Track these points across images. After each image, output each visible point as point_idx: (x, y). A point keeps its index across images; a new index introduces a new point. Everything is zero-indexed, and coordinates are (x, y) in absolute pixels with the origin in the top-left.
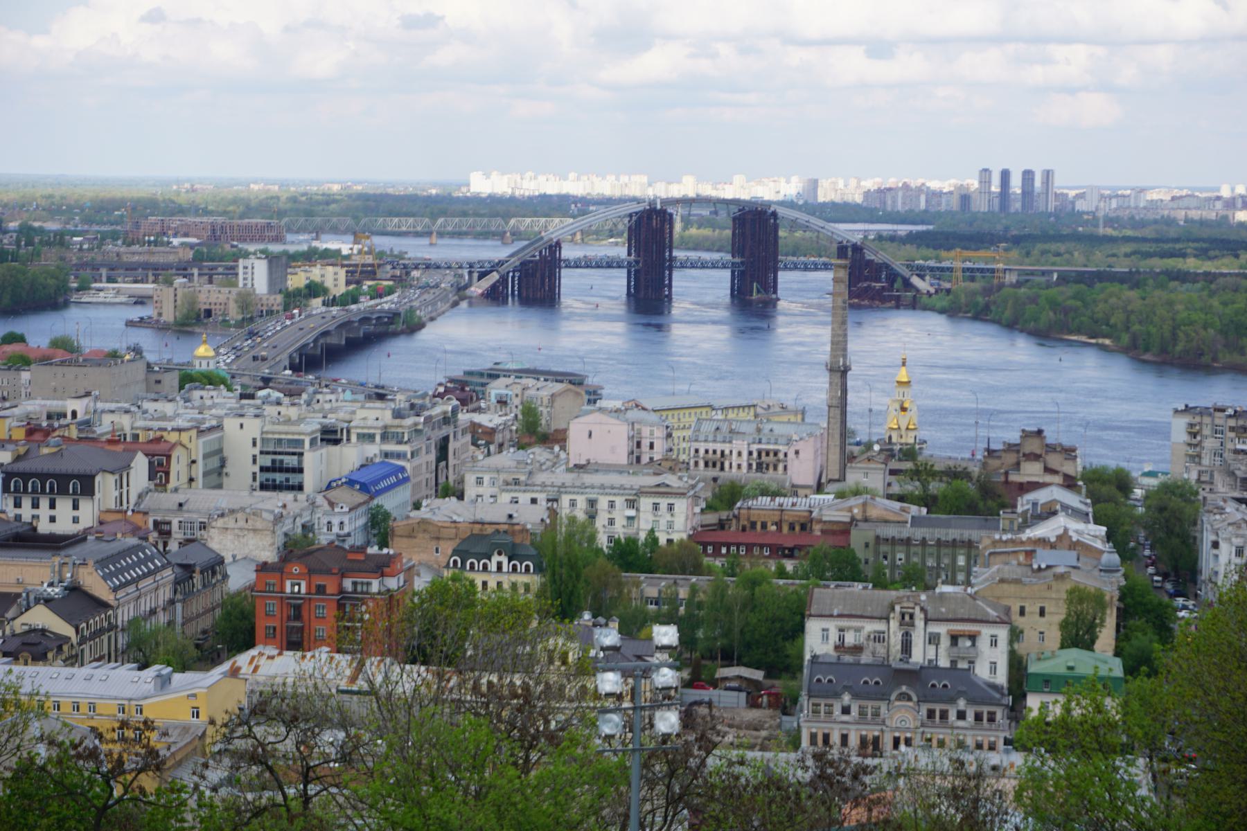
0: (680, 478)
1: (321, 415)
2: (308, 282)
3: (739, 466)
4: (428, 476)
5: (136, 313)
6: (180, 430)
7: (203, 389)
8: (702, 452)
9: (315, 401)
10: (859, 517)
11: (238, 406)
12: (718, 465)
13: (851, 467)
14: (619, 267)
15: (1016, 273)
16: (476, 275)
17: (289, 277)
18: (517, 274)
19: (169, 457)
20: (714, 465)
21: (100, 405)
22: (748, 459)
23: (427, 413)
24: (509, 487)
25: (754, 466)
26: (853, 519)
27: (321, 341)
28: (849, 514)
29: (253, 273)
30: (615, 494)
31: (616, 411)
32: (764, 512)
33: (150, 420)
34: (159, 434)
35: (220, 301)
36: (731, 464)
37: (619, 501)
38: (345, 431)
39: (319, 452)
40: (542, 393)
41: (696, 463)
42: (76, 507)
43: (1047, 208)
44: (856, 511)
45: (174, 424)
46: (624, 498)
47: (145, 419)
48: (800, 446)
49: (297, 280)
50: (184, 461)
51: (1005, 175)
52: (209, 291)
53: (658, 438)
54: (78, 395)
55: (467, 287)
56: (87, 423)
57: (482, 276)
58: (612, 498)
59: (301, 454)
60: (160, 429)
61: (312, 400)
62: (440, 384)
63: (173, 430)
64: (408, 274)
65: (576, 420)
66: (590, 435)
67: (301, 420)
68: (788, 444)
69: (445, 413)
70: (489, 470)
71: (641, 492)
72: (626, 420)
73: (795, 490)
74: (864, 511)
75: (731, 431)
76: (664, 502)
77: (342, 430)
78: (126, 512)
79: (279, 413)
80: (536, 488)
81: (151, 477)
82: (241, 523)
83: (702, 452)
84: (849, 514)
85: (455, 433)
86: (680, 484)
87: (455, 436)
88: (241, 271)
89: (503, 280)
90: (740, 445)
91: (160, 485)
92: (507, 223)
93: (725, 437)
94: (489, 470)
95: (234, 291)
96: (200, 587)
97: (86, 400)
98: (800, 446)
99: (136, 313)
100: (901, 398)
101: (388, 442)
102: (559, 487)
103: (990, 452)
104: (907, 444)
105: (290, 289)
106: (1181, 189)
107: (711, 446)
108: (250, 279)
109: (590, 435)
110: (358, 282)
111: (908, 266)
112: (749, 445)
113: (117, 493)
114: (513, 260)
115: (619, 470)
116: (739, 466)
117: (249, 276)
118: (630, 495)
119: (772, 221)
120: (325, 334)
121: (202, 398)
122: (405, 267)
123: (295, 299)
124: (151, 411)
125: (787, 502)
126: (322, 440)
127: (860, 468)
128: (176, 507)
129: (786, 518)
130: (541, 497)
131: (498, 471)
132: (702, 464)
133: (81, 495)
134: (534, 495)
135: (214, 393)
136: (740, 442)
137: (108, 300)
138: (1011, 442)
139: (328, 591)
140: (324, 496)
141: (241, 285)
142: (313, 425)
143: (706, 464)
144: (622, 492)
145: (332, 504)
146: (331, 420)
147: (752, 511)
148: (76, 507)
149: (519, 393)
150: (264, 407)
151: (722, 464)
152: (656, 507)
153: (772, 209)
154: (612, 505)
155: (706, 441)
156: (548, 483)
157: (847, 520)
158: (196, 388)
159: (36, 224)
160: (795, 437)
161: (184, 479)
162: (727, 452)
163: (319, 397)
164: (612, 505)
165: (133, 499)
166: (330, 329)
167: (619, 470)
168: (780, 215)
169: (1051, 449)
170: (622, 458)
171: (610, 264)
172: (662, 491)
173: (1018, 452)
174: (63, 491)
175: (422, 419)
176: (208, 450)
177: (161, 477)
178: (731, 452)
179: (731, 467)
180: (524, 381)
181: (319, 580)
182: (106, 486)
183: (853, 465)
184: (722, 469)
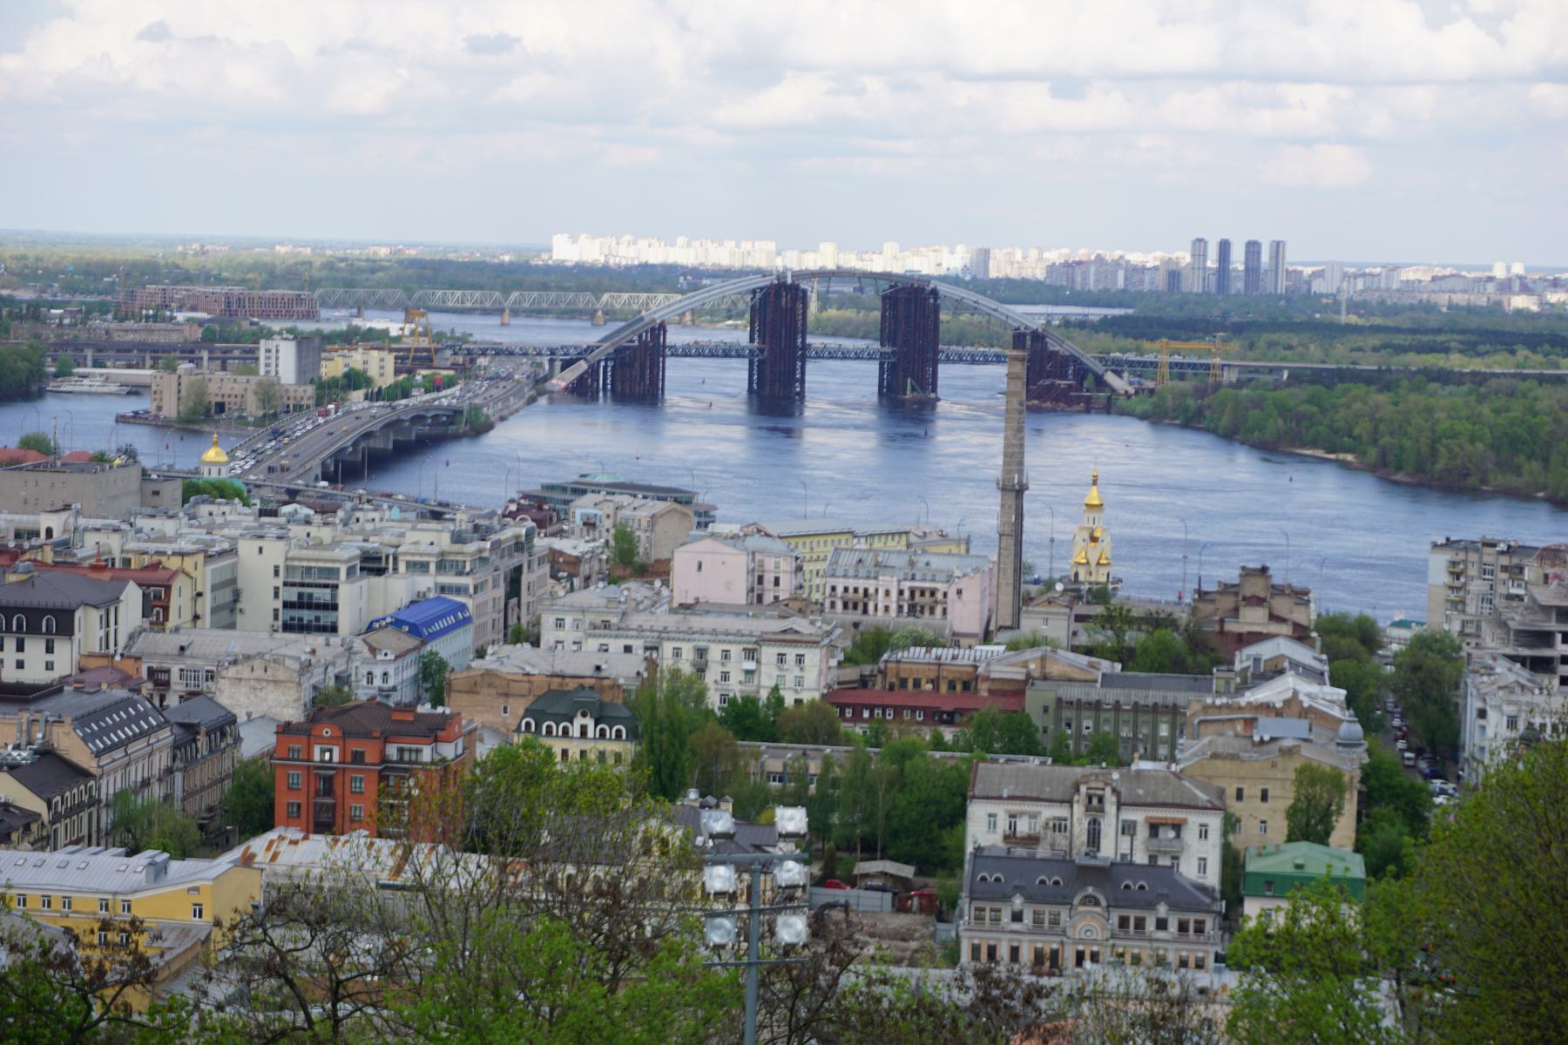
0: (812, 623)
2: (346, 369)
3: (887, 609)
5: (129, 406)
6: (182, 554)
8: (840, 590)
9: (354, 520)
10: (1036, 674)
12: (861, 607)
13: (1027, 612)
14: (739, 356)
15: (1237, 370)
17: (323, 363)
18: (610, 364)
19: (168, 588)
20: (855, 607)
21: (82, 522)
23: (494, 537)
24: (597, 631)
25: (906, 609)
26: (1029, 676)
28: (1024, 670)
29: (277, 358)
30: (729, 642)
31: (732, 538)
32: (917, 667)
34: (156, 559)
36: (876, 606)
37: (736, 651)
39: (358, 584)
40: (639, 513)
41: (833, 604)
42: (50, 650)
43: (1276, 289)
44: (1032, 666)
45: (175, 547)
46: (741, 647)
47: (139, 540)
49: (333, 367)
50: (188, 593)
51: (1224, 247)
56: (66, 544)
57: (566, 365)
59: (336, 587)
60: (158, 553)
62: (512, 501)
64: (473, 361)
67: (335, 543)
70: (572, 609)
71: (763, 640)
72: (746, 549)
73: (956, 639)
74: (1043, 667)
75: (877, 565)
76: (791, 653)
77: (387, 557)
79: (308, 535)
80: (630, 633)
82: (259, 673)
83: (840, 590)
84: (1024, 670)
86: (812, 630)
89: (593, 370)
90: (888, 582)
92: (598, 299)
94: (572, 609)
95: (254, 379)
96: (205, 753)
97: (64, 515)
98: (962, 584)
99: (129, 406)
100: (1091, 525)
102: (660, 632)
103: (1202, 595)
104: (1097, 583)
105: (325, 378)
106: (1444, 267)
107: (851, 583)
112: (899, 581)
113: (102, 633)
114: (605, 345)
115: (736, 611)
116: (887, 609)
117: (273, 362)
118: (749, 643)
119: (932, 301)
120: (368, 435)
123: (330, 391)
125: (946, 654)
126: (362, 569)
127: (1038, 613)
128: (176, 651)
129: (945, 674)
130: (638, 645)
132: (839, 605)
134: (629, 642)
135: (226, 509)
137: (93, 389)
139: (367, 760)
140: (364, 640)
141: (262, 372)
142: (350, 550)
143: (845, 606)
144: (738, 639)
146: (374, 544)
147: (902, 666)
148: (50, 650)
150: (289, 527)
151: (866, 606)
152: (781, 658)
154: (726, 655)
155: (845, 576)
156: (646, 626)
158: (203, 502)
160: (958, 573)
162: (871, 591)
163: (358, 514)
164: (726, 655)
165: (122, 641)
166: (374, 429)
167: (736, 611)
168: (941, 293)
169: (1278, 591)
170: (739, 596)
172: (789, 638)
173: (1236, 594)
174: (34, 630)
175: (488, 545)
177: (158, 613)
179: (876, 609)
180: (618, 498)
181: (355, 746)
182: (88, 623)
183: (1030, 608)
184: (865, 611)
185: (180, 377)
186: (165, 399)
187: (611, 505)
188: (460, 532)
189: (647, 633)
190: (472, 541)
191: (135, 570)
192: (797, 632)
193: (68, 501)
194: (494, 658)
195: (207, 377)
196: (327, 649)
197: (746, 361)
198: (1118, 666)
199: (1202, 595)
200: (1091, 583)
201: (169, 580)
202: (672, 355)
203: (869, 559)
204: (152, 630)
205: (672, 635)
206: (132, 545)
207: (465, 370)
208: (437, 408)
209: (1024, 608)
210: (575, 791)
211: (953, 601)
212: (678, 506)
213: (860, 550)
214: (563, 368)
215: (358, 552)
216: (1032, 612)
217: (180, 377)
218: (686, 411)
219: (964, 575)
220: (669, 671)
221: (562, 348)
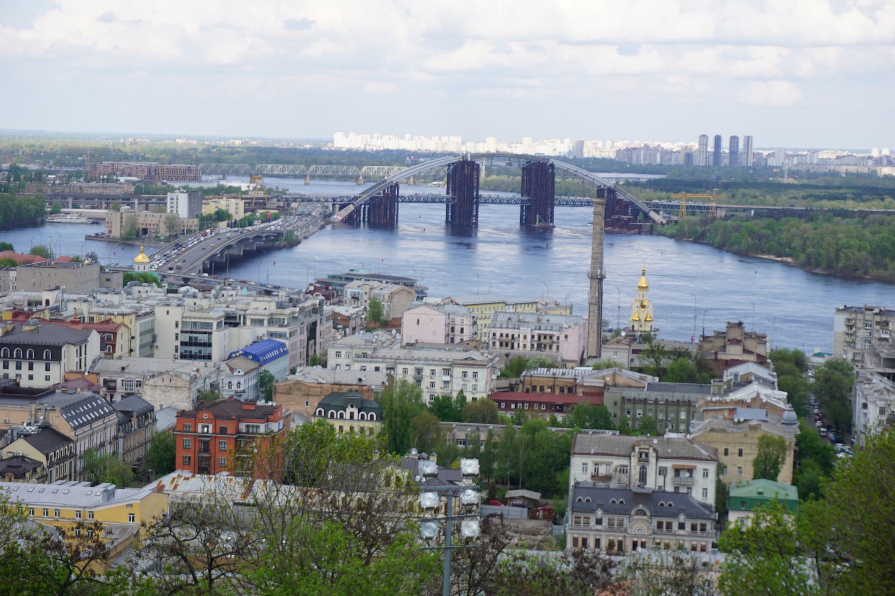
0: (482, 354)
1: (225, 305)
3: (525, 346)
4: (302, 350)
6: (123, 315)
8: (498, 335)
9: (221, 295)
10: (610, 383)
11: (165, 298)
12: (510, 345)
13: (605, 348)
16: (337, 207)
17: (203, 206)
18: (367, 206)
19: (115, 334)
21: (66, 296)
22: (531, 341)
23: (301, 305)
24: (359, 359)
25: (536, 346)
26: (606, 385)
27: (226, 252)
28: (603, 381)
29: (177, 203)
30: (435, 365)
31: (437, 306)
33: (102, 307)
34: (108, 317)
35: (153, 222)
36: (519, 344)
37: (439, 370)
39: (223, 332)
41: (494, 344)
42: (48, 369)
43: (747, 164)
44: (608, 379)
47: (98, 307)
48: (568, 332)
49: (209, 208)
50: (126, 337)
51: (718, 139)
53: (466, 325)
57: (342, 207)
58: (433, 368)
59: (210, 333)
60: (109, 314)
61: (218, 295)
62: (311, 285)
64: (289, 205)
65: (408, 312)
66: (418, 323)
67: (210, 309)
70: (345, 346)
71: (454, 364)
73: (564, 364)
74: (614, 379)
75: (519, 321)
76: (470, 371)
77: (240, 316)
78: (84, 373)
79: (195, 304)
80: (379, 360)
82: (167, 382)
83: (498, 335)
84: (603, 381)
85: (321, 319)
86: (482, 358)
87: (321, 322)
88: (169, 201)
89: (357, 210)
90: (525, 331)
92: (360, 169)
94: (345, 346)
95: (164, 215)
96: (136, 428)
97: (56, 292)
98: (568, 332)
100: (641, 298)
102: (396, 359)
103: (705, 338)
104: (645, 332)
106: (843, 151)
107: (505, 332)
108: (175, 207)
109: (418, 323)
111: (647, 204)
112: (532, 330)
113: (77, 359)
114: (364, 196)
115: (439, 347)
116: (525, 346)
118: (446, 365)
119: (550, 170)
120: (229, 247)
121: (139, 292)
122: (287, 200)
124: (103, 301)
125: (559, 372)
126: (226, 323)
127: (611, 348)
128: (120, 370)
129: (558, 383)
130: (383, 366)
131: (352, 347)
132: (498, 344)
134: (377, 365)
135: (148, 289)
137: (73, 221)
139: (229, 432)
140: (227, 364)
141: (169, 211)
142: (219, 312)
143: (501, 344)
144: (440, 363)
146: (232, 309)
147: (534, 379)
148: (48, 369)
150: (184, 299)
151: (513, 344)
152: (465, 374)
154: (433, 372)
155: (501, 327)
157: (602, 385)
158: (135, 285)
160: (565, 326)
161: (126, 350)
162: (516, 336)
163: (224, 292)
164: (433, 372)
166: (232, 243)
167: (439, 347)
168: (556, 166)
169: (748, 336)
170: (441, 339)
171: (434, 200)
172: (469, 363)
173: (724, 338)
174: (39, 357)
175: (297, 309)
176: (143, 330)
177: (109, 348)
178: (519, 335)
179: (519, 346)
180: (371, 283)
182: (69, 354)
183: (607, 346)
184: (512, 347)
187: (367, 287)
189: (388, 360)
194: (301, 374)
197: (445, 205)
199: (705, 338)
200: (641, 332)
201: (116, 329)
203: (515, 318)
209: (603, 346)
212: (406, 288)
214: (340, 209)
218: (410, 233)
219: (569, 327)
221: (340, 197)
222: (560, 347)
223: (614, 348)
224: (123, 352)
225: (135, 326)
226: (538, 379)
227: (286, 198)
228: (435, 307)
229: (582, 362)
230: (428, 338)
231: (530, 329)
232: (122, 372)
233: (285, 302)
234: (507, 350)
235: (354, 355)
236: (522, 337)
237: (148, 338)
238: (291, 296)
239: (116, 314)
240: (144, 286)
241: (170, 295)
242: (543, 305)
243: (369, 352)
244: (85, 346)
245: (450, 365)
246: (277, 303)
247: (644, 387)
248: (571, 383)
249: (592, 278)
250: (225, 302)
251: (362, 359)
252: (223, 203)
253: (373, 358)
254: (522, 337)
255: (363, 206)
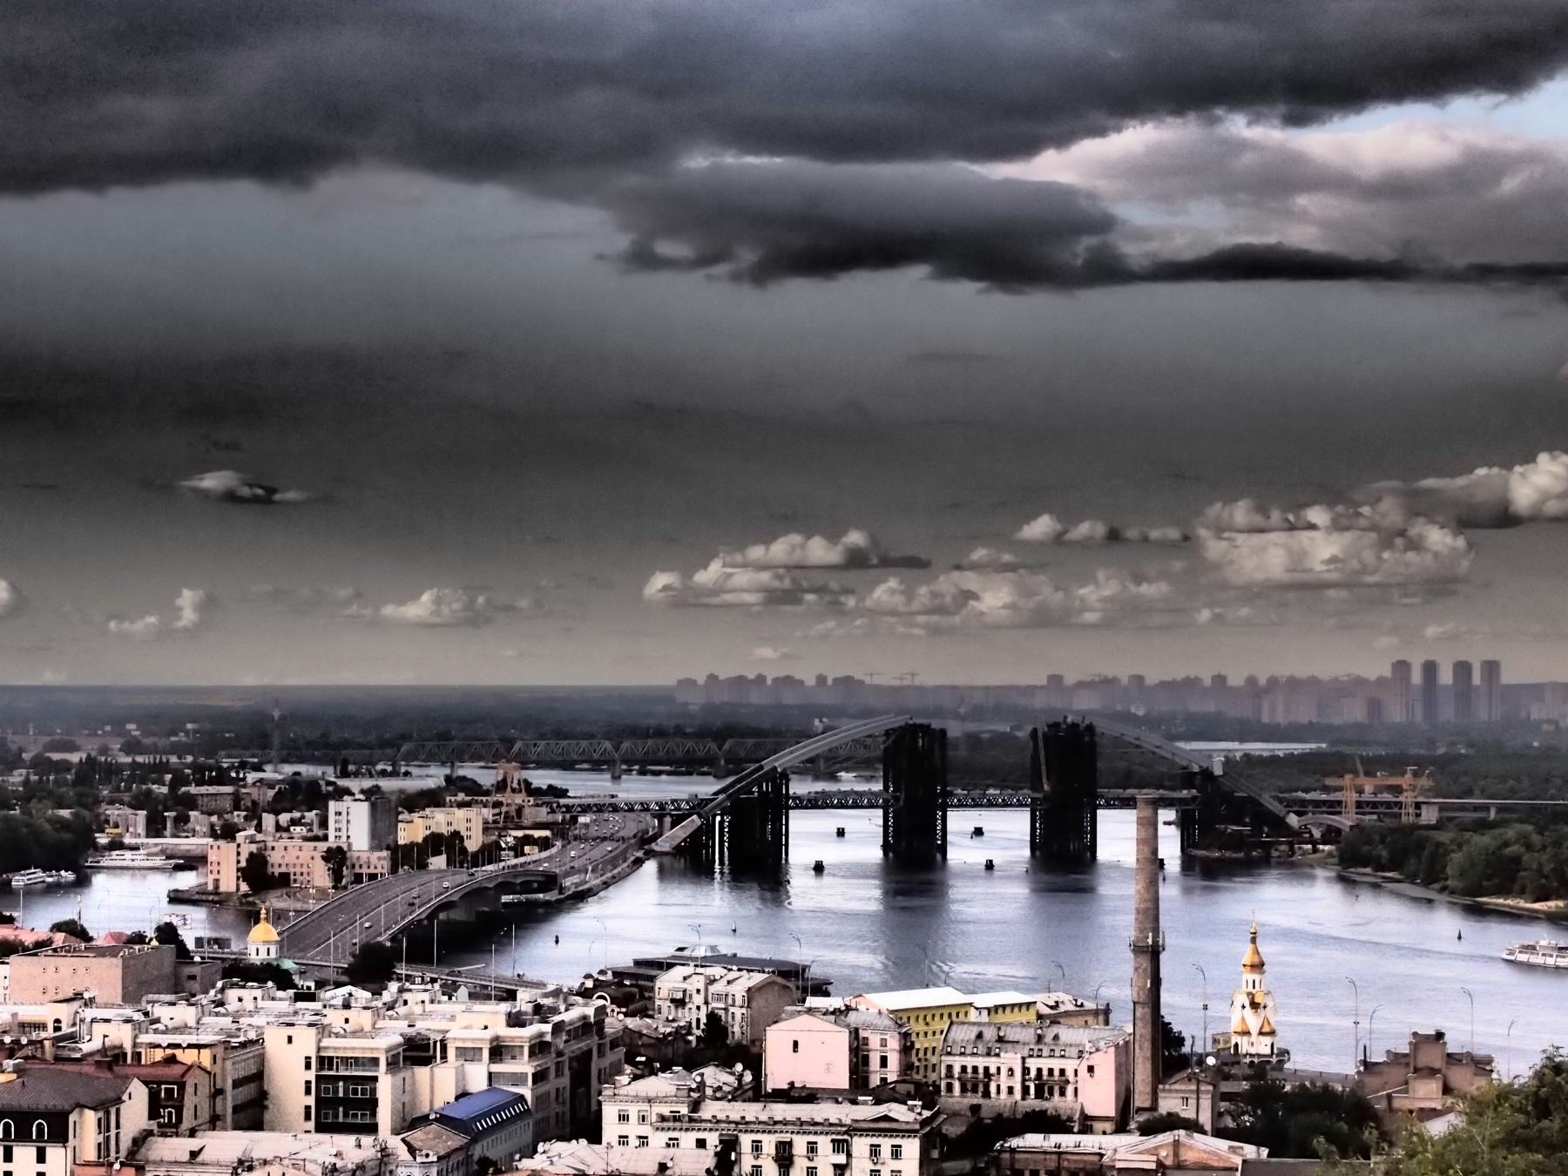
0: (911, 1109)
1: (406, 1023)
2: (428, 832)
3: (1011, 1090)
4: (559, 1109)
5: (187, 881)
6: (199, 1047)
7: (244, 987)
8: (957, 1070)
9: (401, 1002)
10: (1169, 1162)
11: (291, 1010)
12: (981, 1088)
13: (1164, 1090)
14: (871, 806)
15: (1436, 808)
16: (668, 820)
17: (400, 825)
18: (727, 819)
19: (182, 1086)
20: (975, 1090)
21: (89, 1014)
22: (1024, 1081)
23: (557, 1019)
24: (665, 1124)
25: (1032, 1091)
26: (1160, 1164)
27: (442, 916)
28: (1154, 1158)
29: (348, 822)
30: (816, 1133)
31: (833, 1013)
32: (1034, 1156)
33: (164, 1033)
34: (169, 1051)
35: (300, 861)
36: (998, 1086)
37: (824, 1143)
38: (438, 1044)
39: (402, 1075)
40: (732, 989)
41: (950, 1088)
42: (41, 1158)
43: (1490, 717)
44: (1163, 1153)
45: (193, 1039)
46: (830, 1137)
47: (156, 1031)
48: (1095, 1060)
49: (412, 830)
50: (204, 1091)
51: (1430, 669)
52: (286, 848)
53: (892, 1050)
54: (60, 997)
55: (654, 838)
56: (72, 1037)
57: (677, 821)
58: (812, 1138)
59: (375, 1079)
60: (170, 1046)
61: (395, 1002)
62: (588, 976)
63: (190, 1046)
64: (574, 820)
65: (774, 1027)
66: (796, 1044)
67: (375, 1031)
68: (1079, 1057)
69: (585, 1017)
70: (637, 1099)
71: (855, 1129)
72: (848, 1026)
73: (1087, 1124)
74: (1176, 1154)
75: (1001, 1040)
76: (886, 1144)
77: (435, 1043)
78: (111, 1165)
79: (347, 1021)
80: (704, 1125)
81: (153, 1114)
83: (957, 1070)
84: (1154, 1158)
85: (600, 1046)
86: (910, 1117)
87: (599, 1052)
89: (707, 829)
90: (1010, 1059)
91: (170, 1125)
93: (989, 1049)
94: (637, 1099)
97: (76, 1005)
98: (1095, 1060)
99: (187, 881)
100: (1250, 989)
101: (501, 1061)
102: (737, 1123)
103: (1368, 1066)
104: (1259, 1055)
105: (401, 842)
107: (970, 1062)
108: (344, 830)
110: (1383, 841)
111: (1281, 801)
112: (1023, 1059)
113: (101, 1139)
114: (721, 797)
115: (834, 1096)
116: (1011, 1090)
117: (343, 826)
118: (838, 1133)
119: (1087, 739)
120: (446, 906)
121: (240, 1000)
122: (569, 808)
123: (409, 858)
124: (165, 1020)
125: (1067, 1141)
126: (405, 1058)
127: (1177, 1091)
128: (186, 1157)
129: (1066, 1164)
130: (713, 1139)
131: (649, 1101)
132: (957, 1086)
133: (14, 1141)
134: (701, 1135)
135: (258, 993)
136: (1010, 1055)
137: (136, 864)
138: (1398, 1051)
140: (403, 1140)
141: (331, 838)
142: (391, 1034)
143: (964, 1090)
144: (827, 1129)
145: (412, 1150)
146: (422, 1026)
147: (1018, 1156)
148: (41, 1158)
149: (702, 987)
150: (325, 1012)
151: (987, 1087)
152: (875, 1151)
153: (1087, 722)
154: (812, 1148)
155: (962, 1054)
156: (721, 1116)
157: (1153, 1166)
158: (233, 986)
159: (56, 756)
160: (1088, 1047)
161: (205, 1115)
162: (993, 1070)
163: (406, 996)
164: (812, 1148)
165: (126, 1143)
166: (455, 898)
167: (834, 1096)
168: (1098, 730)
169: (1452, 1059)
170: (840, 1079)
172: (884, 1127)
173: (1407, 1064)
174: (24, 1137)
175: (547, 1028)
176: (242, 1074)
177: (170, 1113)
178: (999, 1069)
179: (998, 1092)
180: (709, 971)
182: (86, 1124)
183: (1167, 1087)
184: (987, 1094)
185: (239, 846)
186: (223, 868)
187: (702, 978)
188: (520, 1013)
189: (723, 1125)
190: (531, 1024)
191: (146, 1066)
192: (896, 1121)
193: (79, 989)
194: (545, 1156)
195: (270, 844)
196: (358, 1150)
197: (880, 812)
198: (1265, 1152)
199: (1368, 1066)
200: (1251, 1055)
201: (183, 1075)
202: (797, 807)
203: (990, 1034)
204: (164, 1135)
205: (753, 1127)
206: (144, 1038)
207: (563, 831)
208: (526, 873)
209: (1161, 1087)
210: (1442, 1155)
211: (1084, 1079)
212: (779, 980)
213: (979, 1024)
214: (673, 826)
215: (401, 1040)
216: (1170, 1091)
217: (239, 846)
219: (1098, 1050)
220: (1091, 1126)
221: (673, 801)
222: (308, 1135)
223: (1181, 1091)
224: (200, 1121)
225: (223, 1069)
226: (1026, 1156)
227: (566, 806)
228: (832, 1018)
229: (1121, 1127)
230: (814, 1080)
231: (1019, 1056)
232: (189, 1162)
233: (526, 1013)
234: (976, 1099)
235: (654, 1118)
236: (1004, 1072)
237: (247, 1092)
238: (539, 1001)
239: (184, 1045)
240: (252, 987)
241: (300, 1005)
242: (1051, 1007)
243: (684, 1110)
244: (118, 1111)
245: (846, 1133)
246: (509, 1015)
247: (1237, 1170)
248: (1092, 1163)
249: (1138, 949)
250: (406, 1017)
251: (671, 1124)
252: (441, 820)
253: (693, 1122)
254: (1004, 1072)
255: (718, 818)
